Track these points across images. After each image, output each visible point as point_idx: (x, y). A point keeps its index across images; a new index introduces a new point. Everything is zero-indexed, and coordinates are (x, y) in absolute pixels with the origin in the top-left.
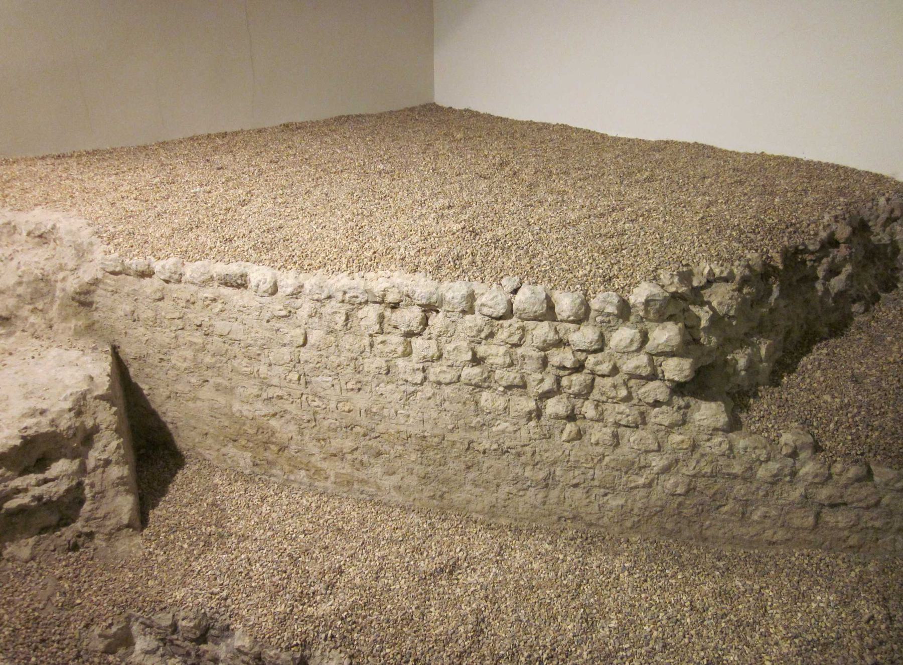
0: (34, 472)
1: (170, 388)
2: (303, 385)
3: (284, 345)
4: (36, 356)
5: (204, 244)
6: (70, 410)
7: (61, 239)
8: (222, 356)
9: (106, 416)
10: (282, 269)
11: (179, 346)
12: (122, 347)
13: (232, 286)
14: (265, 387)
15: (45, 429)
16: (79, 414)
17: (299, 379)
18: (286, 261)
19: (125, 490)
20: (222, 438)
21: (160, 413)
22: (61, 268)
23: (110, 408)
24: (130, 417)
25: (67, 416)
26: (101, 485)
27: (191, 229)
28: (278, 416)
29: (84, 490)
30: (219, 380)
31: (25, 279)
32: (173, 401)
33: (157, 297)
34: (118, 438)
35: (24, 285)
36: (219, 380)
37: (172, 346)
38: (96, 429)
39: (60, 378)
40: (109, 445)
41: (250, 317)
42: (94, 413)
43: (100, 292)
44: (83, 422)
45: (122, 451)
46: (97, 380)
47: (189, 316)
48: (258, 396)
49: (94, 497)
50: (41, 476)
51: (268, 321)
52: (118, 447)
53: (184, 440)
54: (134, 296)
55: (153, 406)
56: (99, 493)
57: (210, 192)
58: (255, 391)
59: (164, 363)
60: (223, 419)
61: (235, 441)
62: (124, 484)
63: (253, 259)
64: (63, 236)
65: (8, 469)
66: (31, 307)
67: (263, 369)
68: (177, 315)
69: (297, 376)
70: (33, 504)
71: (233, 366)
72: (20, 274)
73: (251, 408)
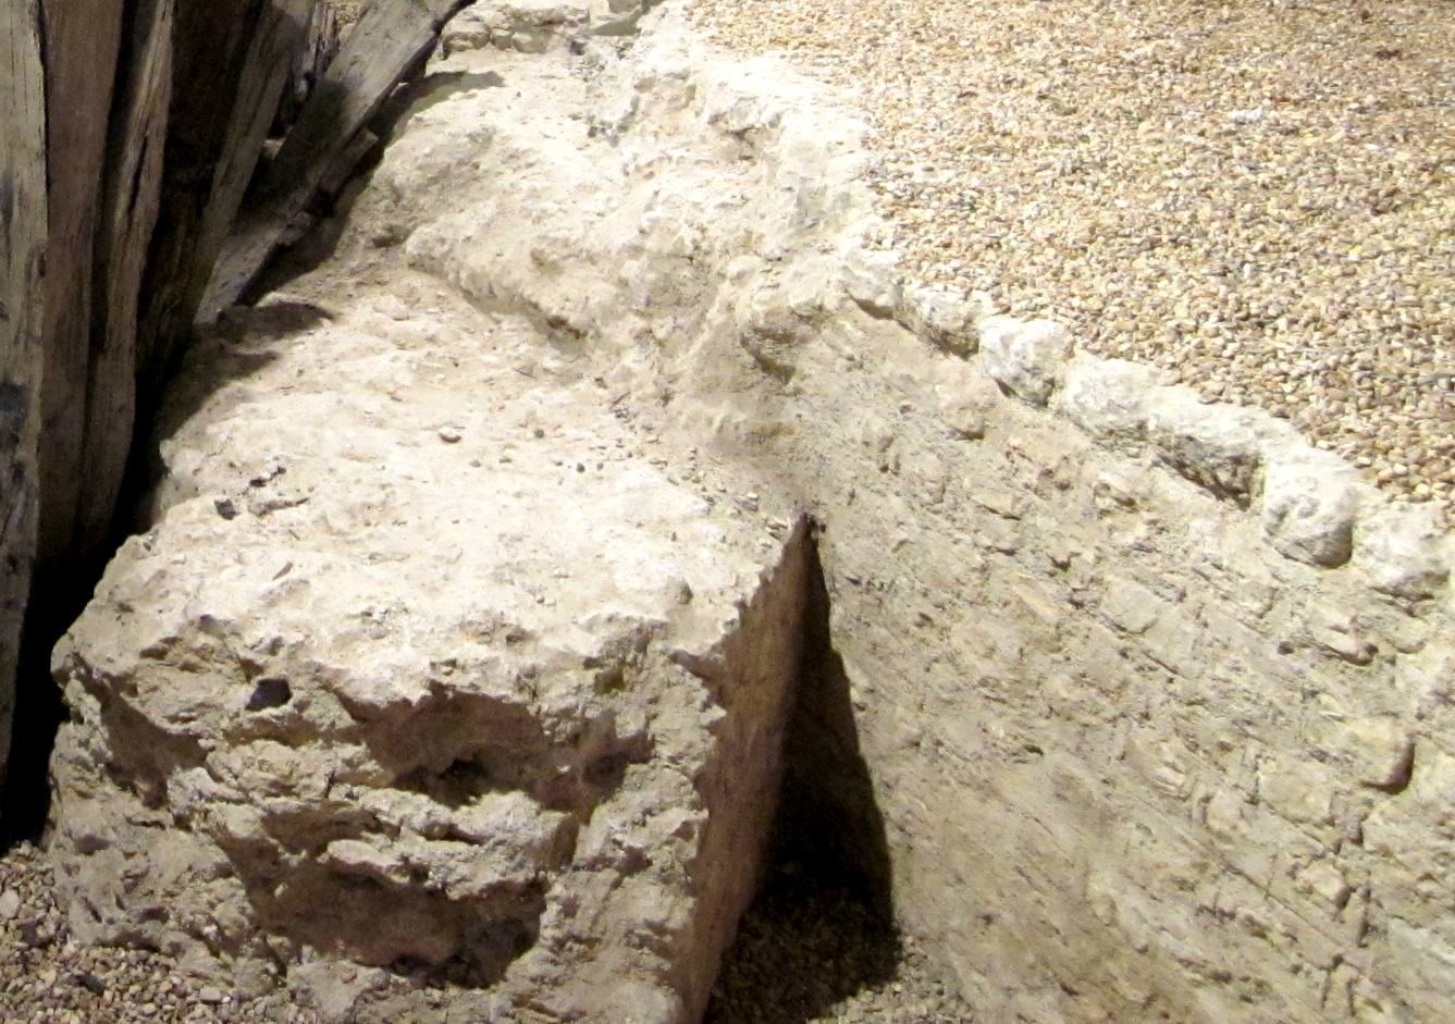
0: (434, 796)
1: (924, 718)
2: (1350, 931)
3: (1322, 756)
4: (590, 469)
5: (1163, 310)
6: (589, 663)
7: (774, 161)
8: (1104, 692)
9: (684, 724)
10: (1390, 490)
11: (986, 601)
12: (831, 530)
13: (1197, 479)
14: (1215, 867)
15: (499, 688)
16: (612, 683)
17: (1343, 901)
18: (1421, 463)
19: (658, 970)
20: (1030, 958)
21: (875, 779)
22: (747, 243)
23: (706, 706)
24: (788, 748)
25: (574, 676)
26: (595, 921)
27: (1154, 244)
28: (1229, 988)
29: (543, 908)
30: (1074, 767)
31: (651, 244)
32: (922, 761)
33: (964, 427)
34: (695, 806)
35: (644, 258)
36: (1074, 767)
37: (966, 592)
38: (641, 749)
39: (609, 555)
40: (654, 812)
41: (1230, 607)
42: (654, 701)
43: (817, 347)
44: (610, 715)
45: (691, 851)
46: (701, 608)
47: (1039, 520)
48: (1183, 884)
49: (560, 944)
50: (443, 813)
51: (1285, 649)
52: (684, 832)
53: (922, 899)
54: (905, 397)
55: (865, 748)
56: (578, 940)
57: (1294, 132)
58: (1180, 864)
59: (926, 633)
60: (1052, 898)
61: (1070, 992)
62: (663, 951)
63: (1305, 414)
64: (784, 156)
65: (374, 754)
66: (640, 324)
67: (1226, 804)
68: (1004, 503)
69: (1332, 888)
70: (397, 878)
71: (1130, 744)
72: (645, 225)
73: (1148, 913)
